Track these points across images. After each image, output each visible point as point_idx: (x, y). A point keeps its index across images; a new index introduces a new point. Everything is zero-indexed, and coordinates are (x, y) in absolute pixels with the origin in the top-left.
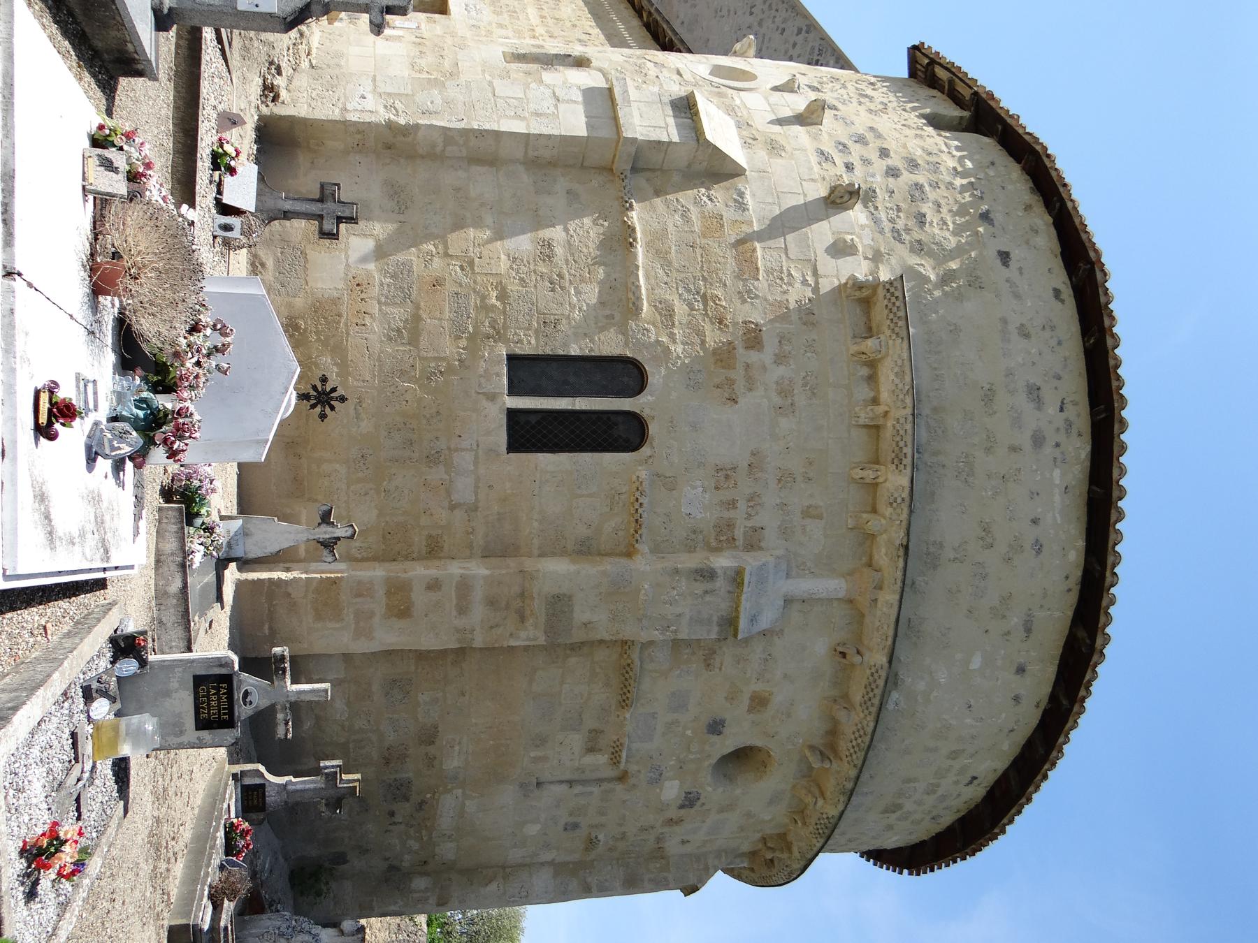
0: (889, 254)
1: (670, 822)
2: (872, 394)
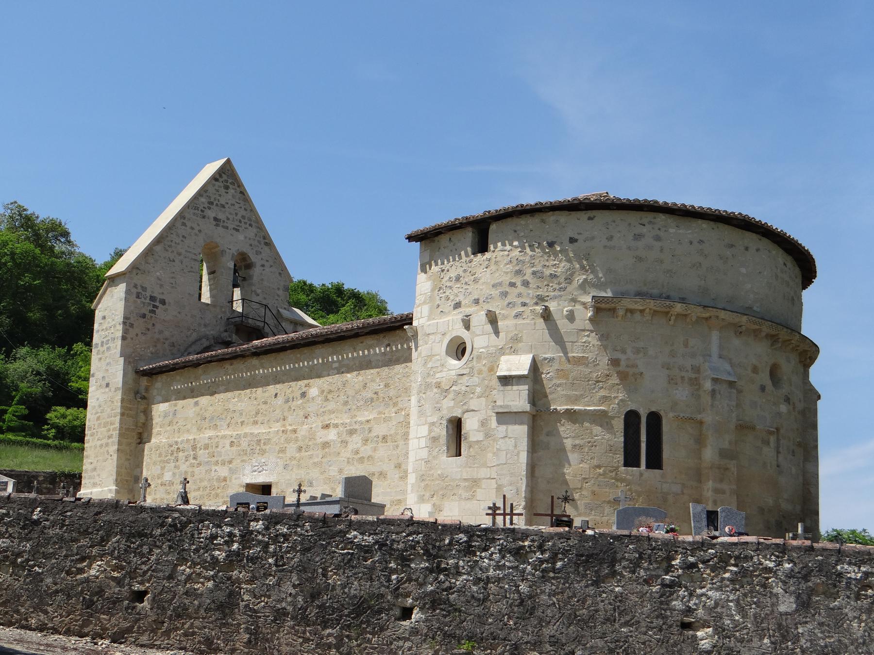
1: (794, 408)
2: (639, 312)
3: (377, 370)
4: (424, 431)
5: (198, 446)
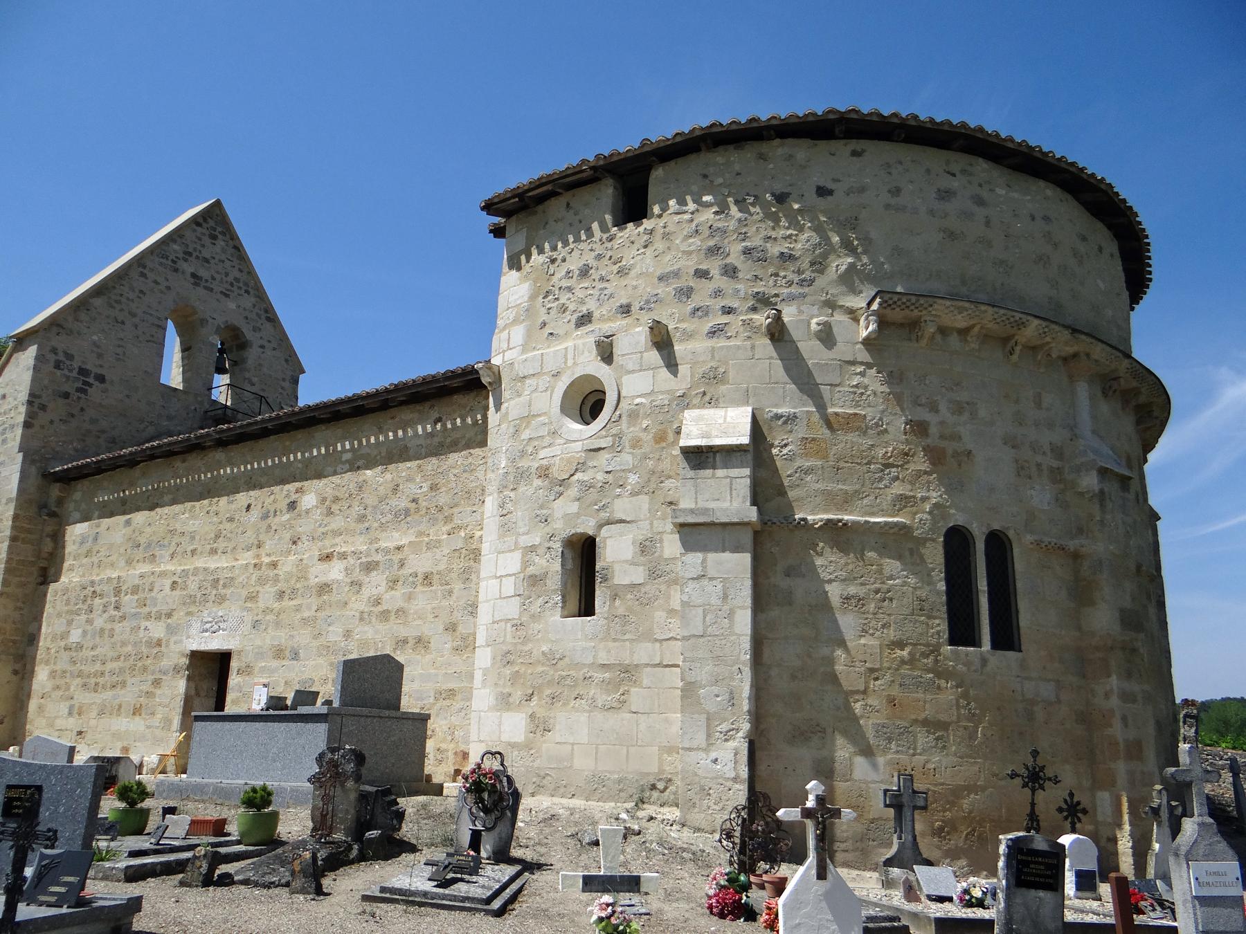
0: (827, 294)
3: (417, 462)
4: (512, 563)
5: (124, 588)
